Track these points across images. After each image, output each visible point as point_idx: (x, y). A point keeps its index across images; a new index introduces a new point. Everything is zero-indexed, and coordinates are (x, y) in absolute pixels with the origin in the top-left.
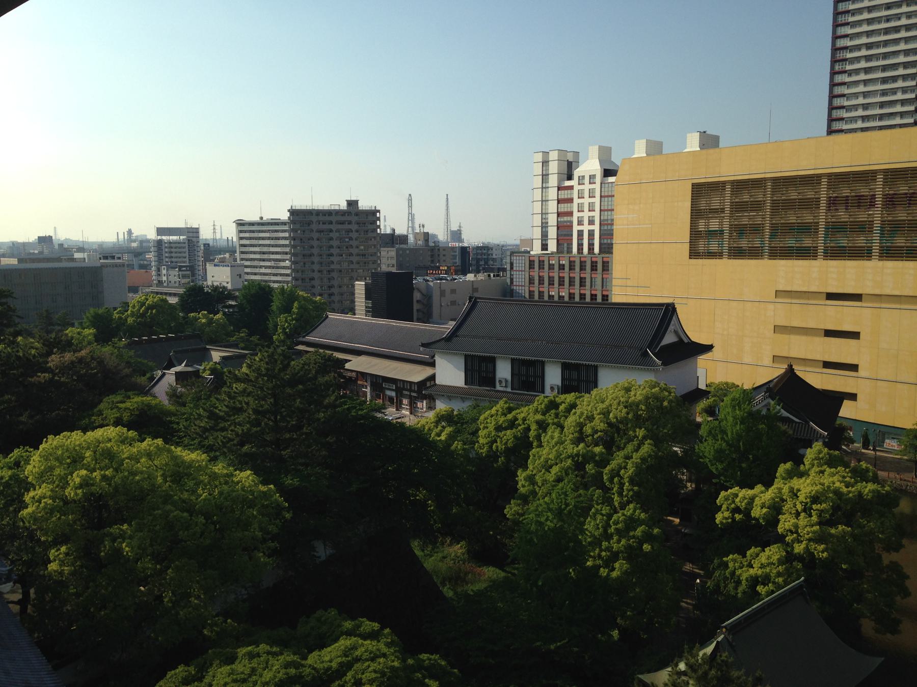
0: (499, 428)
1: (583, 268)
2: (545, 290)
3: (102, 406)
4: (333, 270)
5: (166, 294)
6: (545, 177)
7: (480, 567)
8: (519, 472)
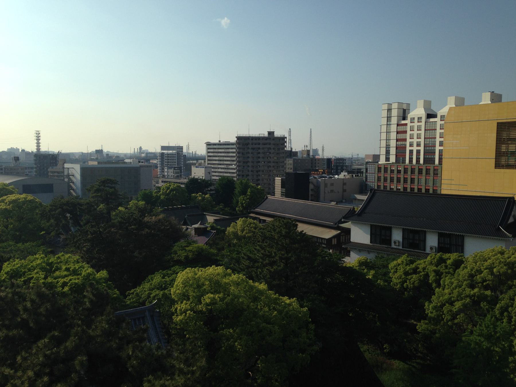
0: (406, 273)
1: (413, 172)
2: (388, 185)
3: (175, 248)
4: (259, 171)
5: (179, 183)
6: (389, 118)
7: (389, 359)
8: (426, 304)
